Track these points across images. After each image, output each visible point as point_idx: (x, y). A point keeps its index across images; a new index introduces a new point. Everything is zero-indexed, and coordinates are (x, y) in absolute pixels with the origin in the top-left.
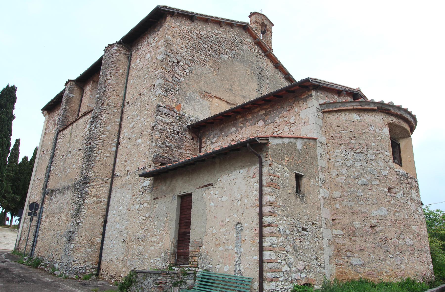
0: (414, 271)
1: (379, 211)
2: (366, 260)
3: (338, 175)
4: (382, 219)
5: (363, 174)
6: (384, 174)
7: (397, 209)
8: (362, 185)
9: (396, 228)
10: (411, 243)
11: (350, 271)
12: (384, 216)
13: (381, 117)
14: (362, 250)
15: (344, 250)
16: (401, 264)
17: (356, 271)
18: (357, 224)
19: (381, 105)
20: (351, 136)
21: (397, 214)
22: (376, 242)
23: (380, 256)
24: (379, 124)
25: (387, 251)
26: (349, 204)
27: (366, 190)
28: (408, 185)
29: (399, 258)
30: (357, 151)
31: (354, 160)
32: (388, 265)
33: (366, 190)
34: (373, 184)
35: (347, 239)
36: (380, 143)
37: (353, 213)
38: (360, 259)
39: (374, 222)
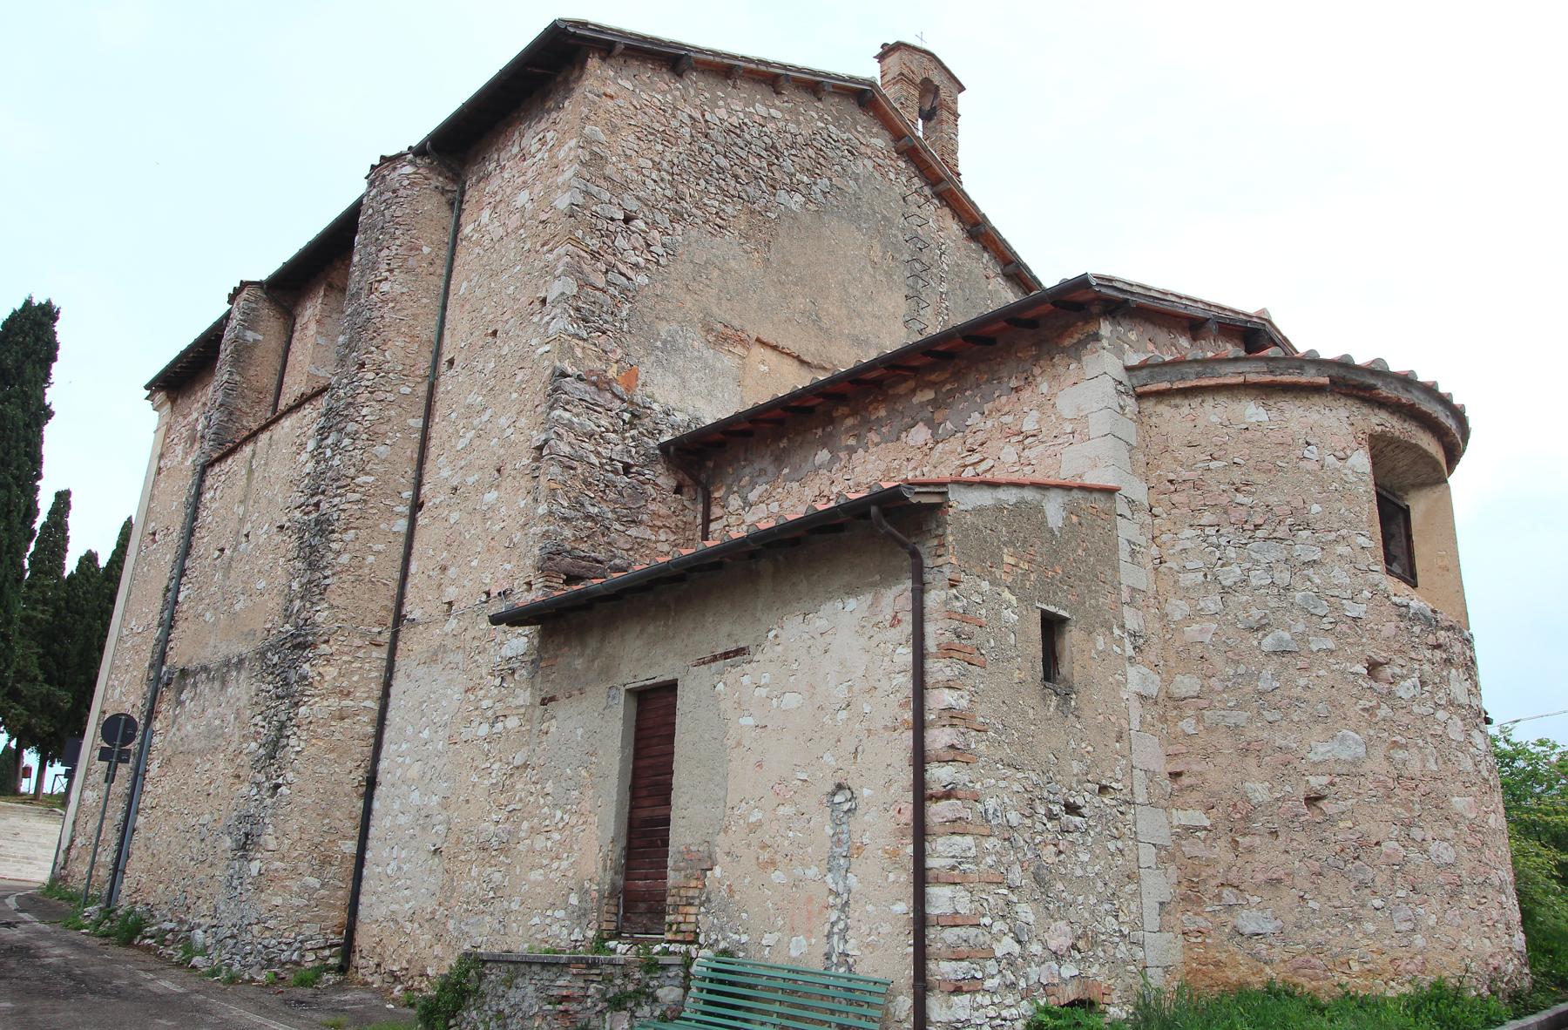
0: (1458, 956)
1: (1335, 744)
2: (1291, 918)
3: (1189, 619)
4: (1344, 771)
5: (1279, 615)
6: (1355, 614)
7: (1398, 738)
8: (1275, 652)
9: (1394, 805)
10: (1448, 856)
11: (1232, 955)
12: (1353, 763)
13: (1343, 413)
14: (1274, 883)
15: (1213, 882)
16: (1413, 930)
17: (1255, 956)
18: (1259, 791)
19: (1342, 372)
20: (1237, 481)
21: (1400, 755)
22: (1324, 853)
23: (1338, 904)
24: (1337, 438)
25: (1362, 885)
26: (1231, 721)
27: (1291, 670)
28: (1438, 653)
29: (1406, 911)
30: (1259, 533)
31: (1248, 565)
32: (1366, 935)
33: (1291, 670)
34: (1315, 649)
35: (1222, 843)
36: (1339, 505)
37: (1245, 751)
38: (1268, 912)
39: (1317, 782)
